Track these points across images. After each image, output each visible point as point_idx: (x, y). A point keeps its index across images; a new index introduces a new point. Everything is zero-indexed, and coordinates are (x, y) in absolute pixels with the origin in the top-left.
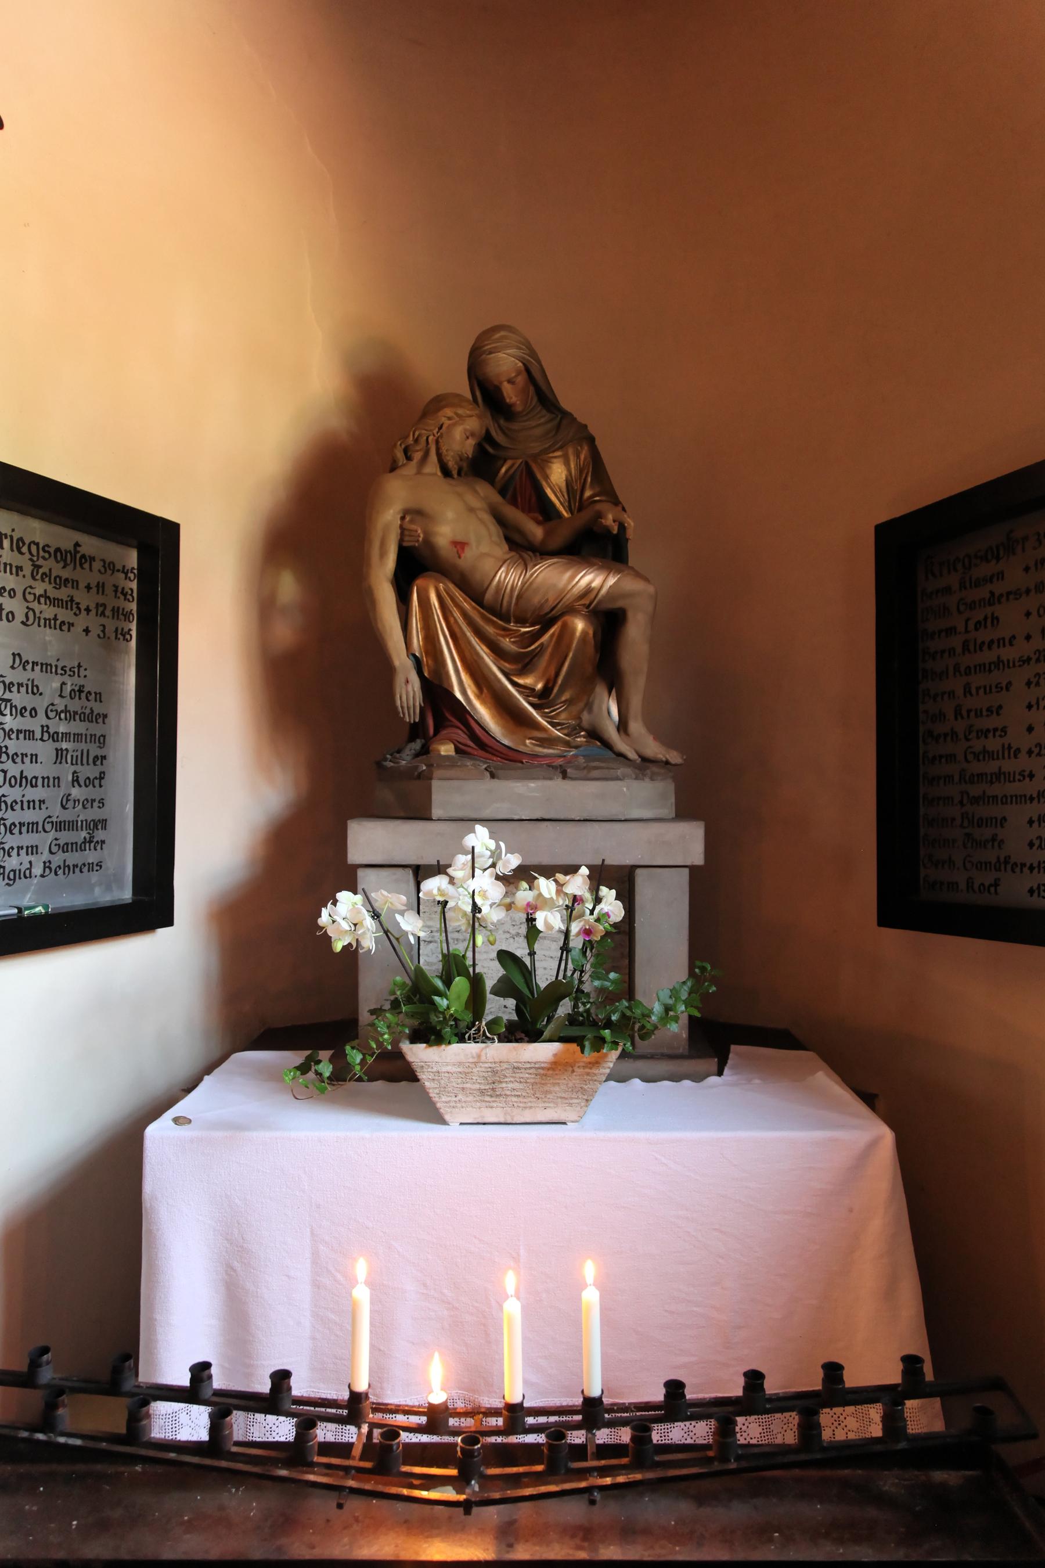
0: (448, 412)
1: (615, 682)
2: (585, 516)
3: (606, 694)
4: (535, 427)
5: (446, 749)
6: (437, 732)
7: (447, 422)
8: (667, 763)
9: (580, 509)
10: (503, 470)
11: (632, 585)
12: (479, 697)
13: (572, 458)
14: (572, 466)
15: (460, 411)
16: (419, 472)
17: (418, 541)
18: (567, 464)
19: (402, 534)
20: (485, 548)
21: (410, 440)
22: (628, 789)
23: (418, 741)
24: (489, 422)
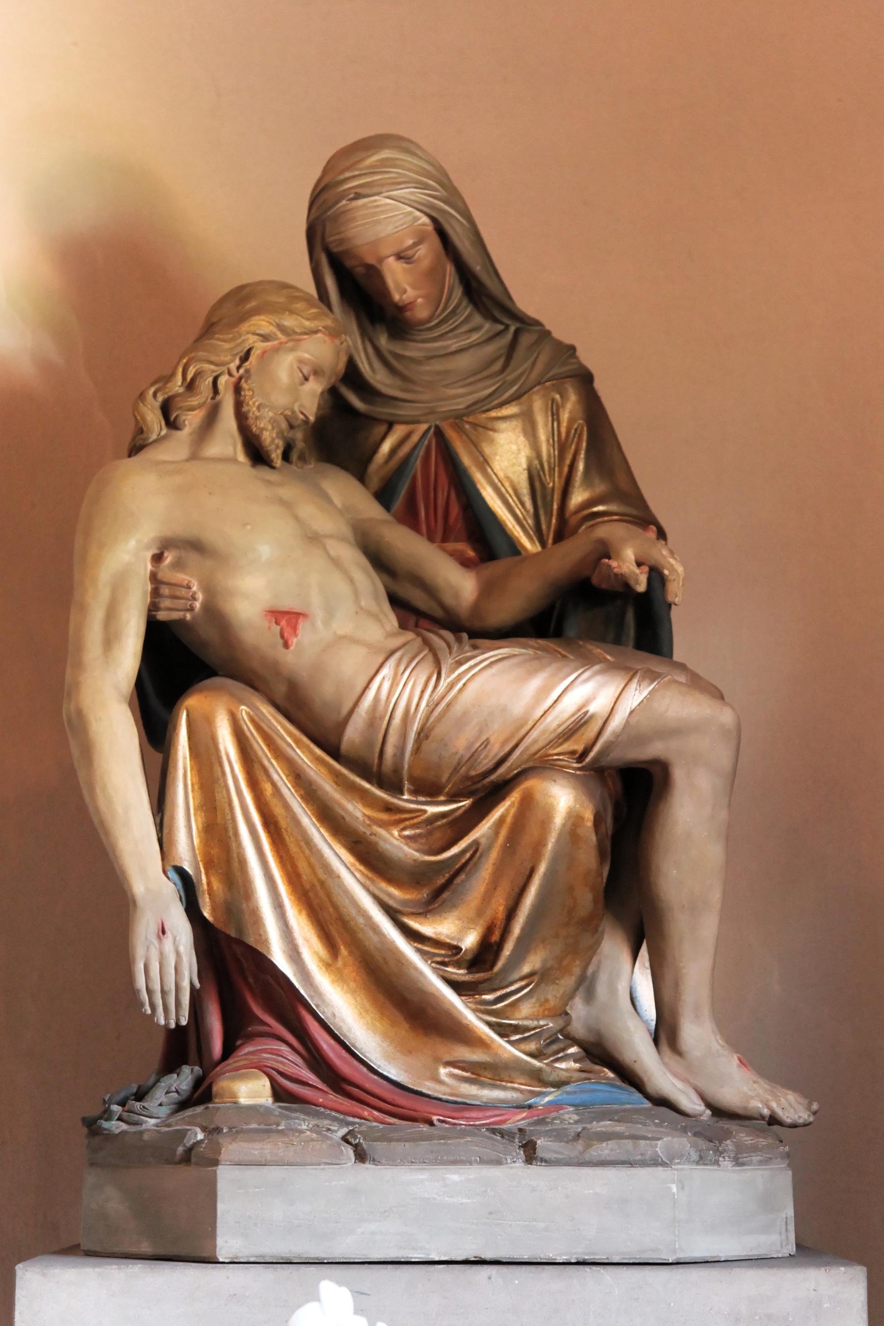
0: (263, 323)
1: (644, 927)
2: (567, 557)
3: (625, 956)
4: (451, 359)
5: (251, 1091)
6: (229, 1050)
7: (260, 346)
8: (773, 1120)
9: (560, 536)
10: (386, 447)
11: (678, 705)
12: (328, 966)
13: (541, 419)
14: (542, 436)
15: (289, 322)
16: (194, 456)
17: (191, 609)
18: (530, 432)
19: (156, 593)
20: (343, 625)
21: (177, 385)
22: (682, 1187)
23: (186, 1070)
24: (353, 340)
